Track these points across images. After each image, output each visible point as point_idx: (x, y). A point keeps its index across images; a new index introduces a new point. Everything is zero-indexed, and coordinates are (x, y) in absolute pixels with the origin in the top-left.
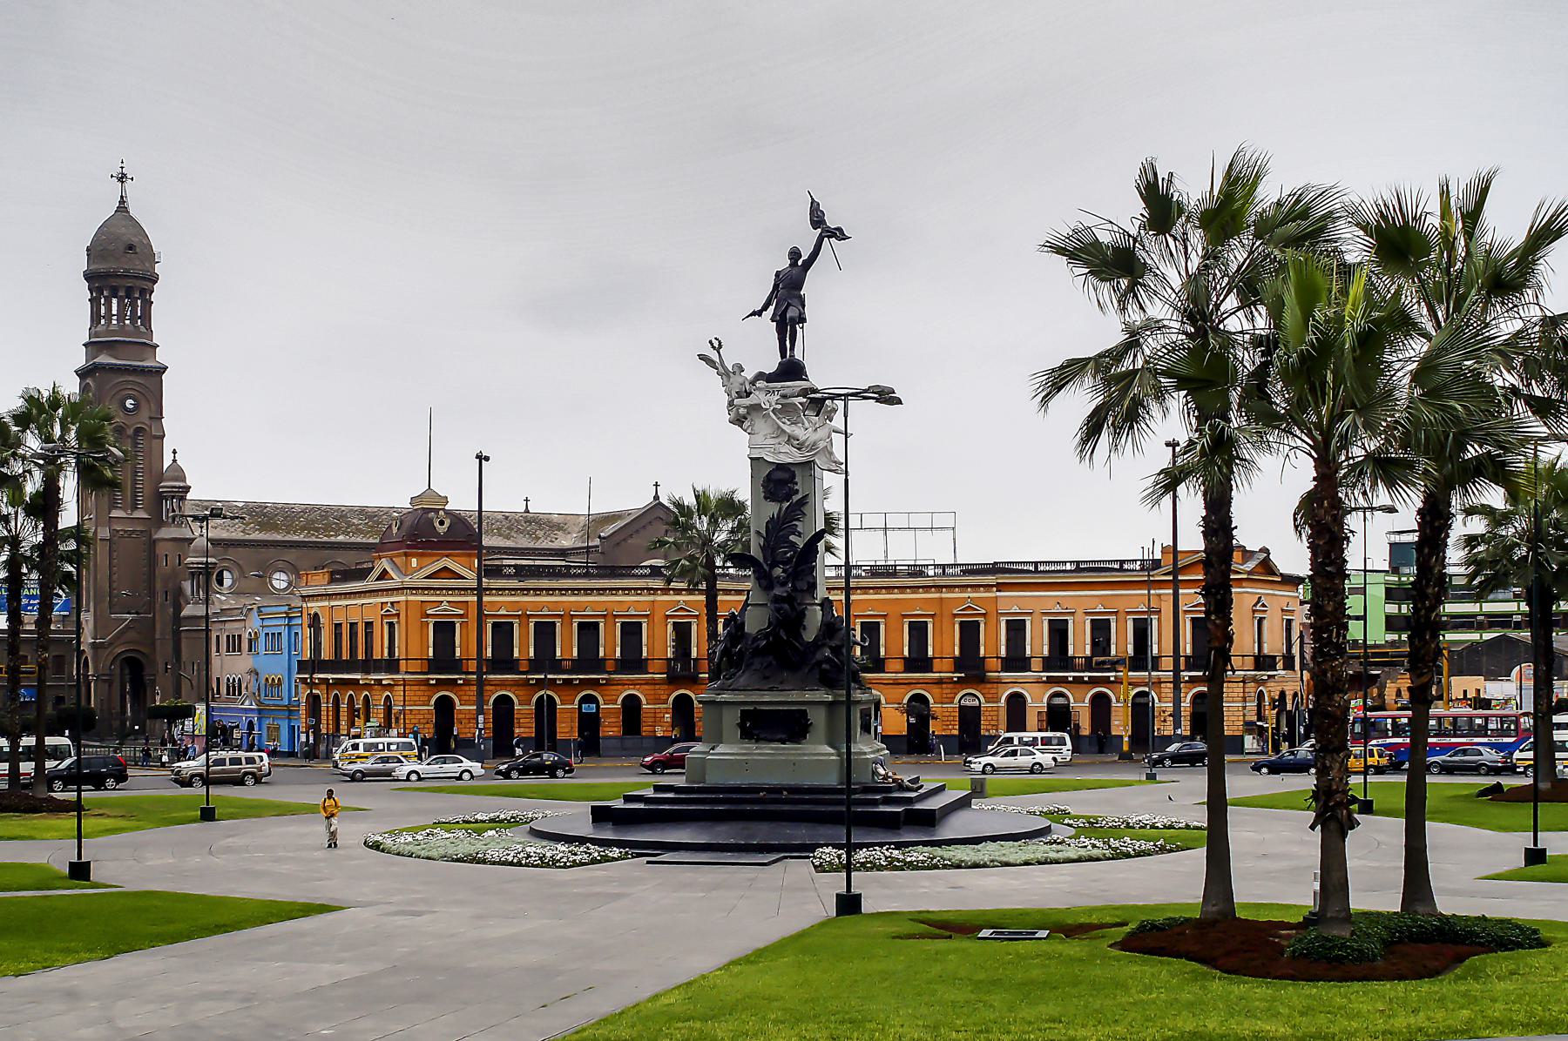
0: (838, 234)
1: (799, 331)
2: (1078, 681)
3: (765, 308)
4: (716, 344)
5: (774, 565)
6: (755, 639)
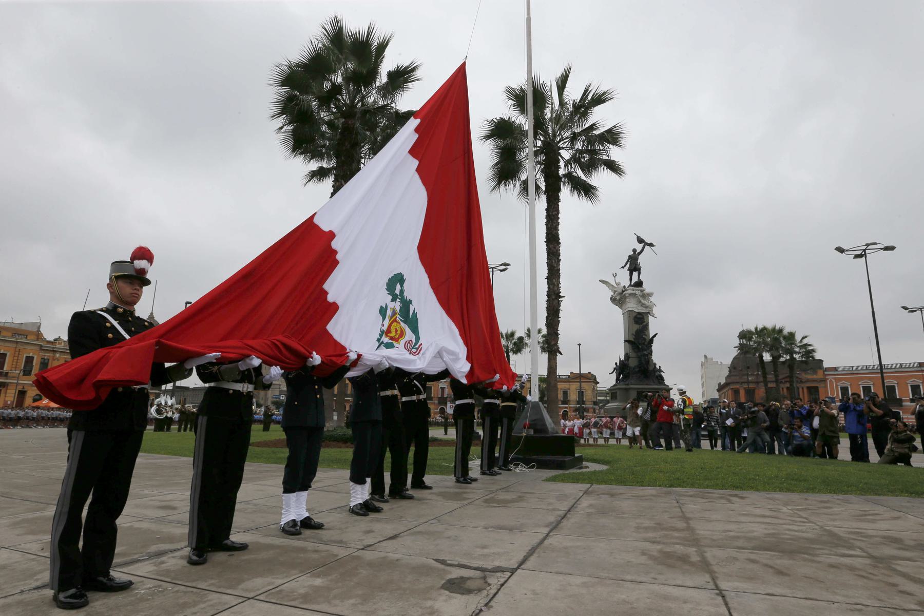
0: (651, 245)
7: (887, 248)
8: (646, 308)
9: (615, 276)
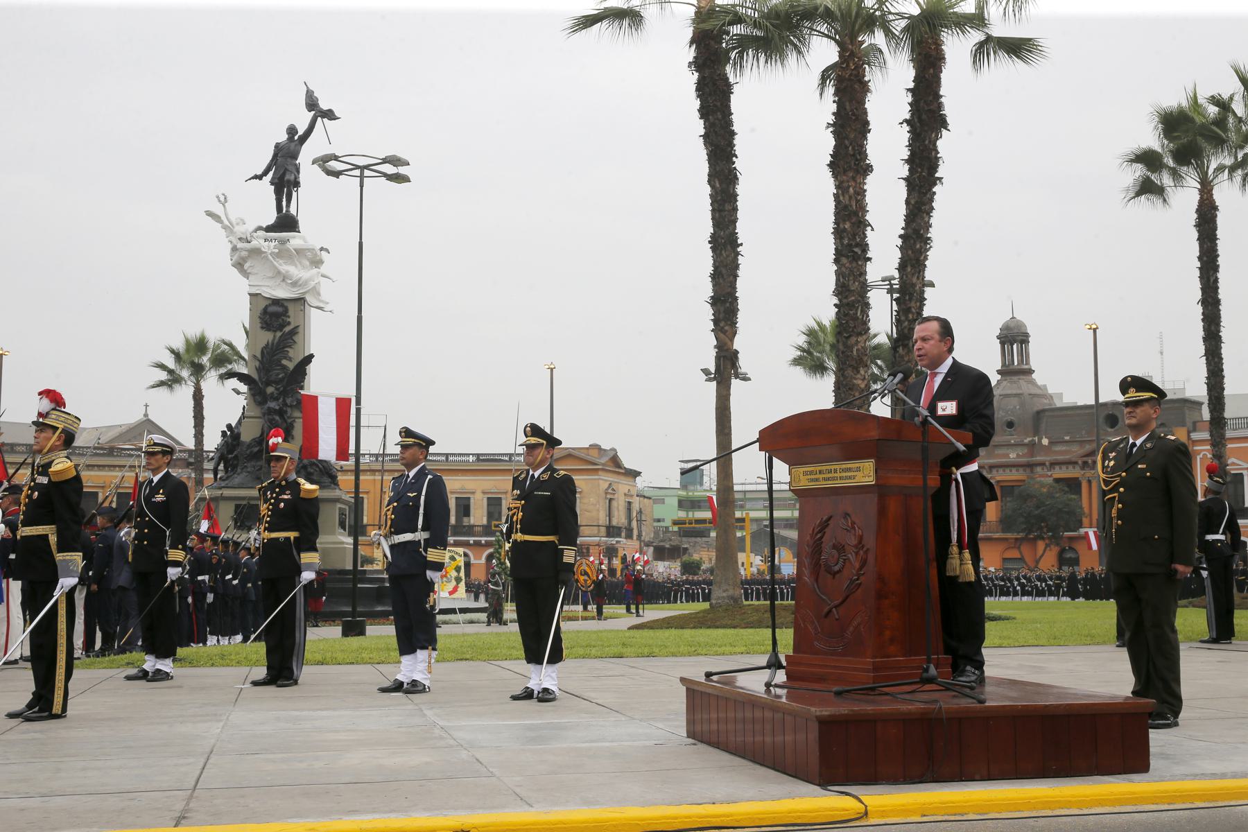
0: (330, 115)
1: (294, 194)
2: (477, 544)
3: (265, 173)
4: (222, 199)
5: (268, 384)
6: (249, 446)
8: (295, 284)
9: (224, 201)
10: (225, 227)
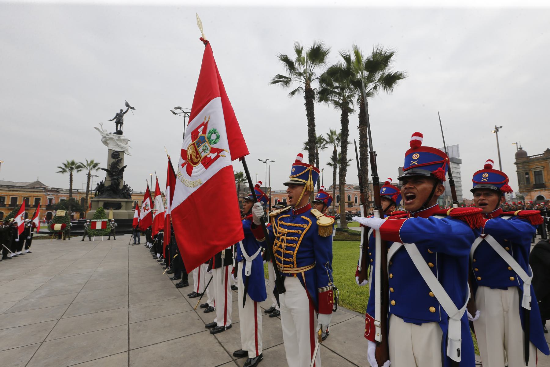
0: (133, 108)
7: (272, 161)
8: (122, 148)
9: (102, 125)
10: (100, 132)
